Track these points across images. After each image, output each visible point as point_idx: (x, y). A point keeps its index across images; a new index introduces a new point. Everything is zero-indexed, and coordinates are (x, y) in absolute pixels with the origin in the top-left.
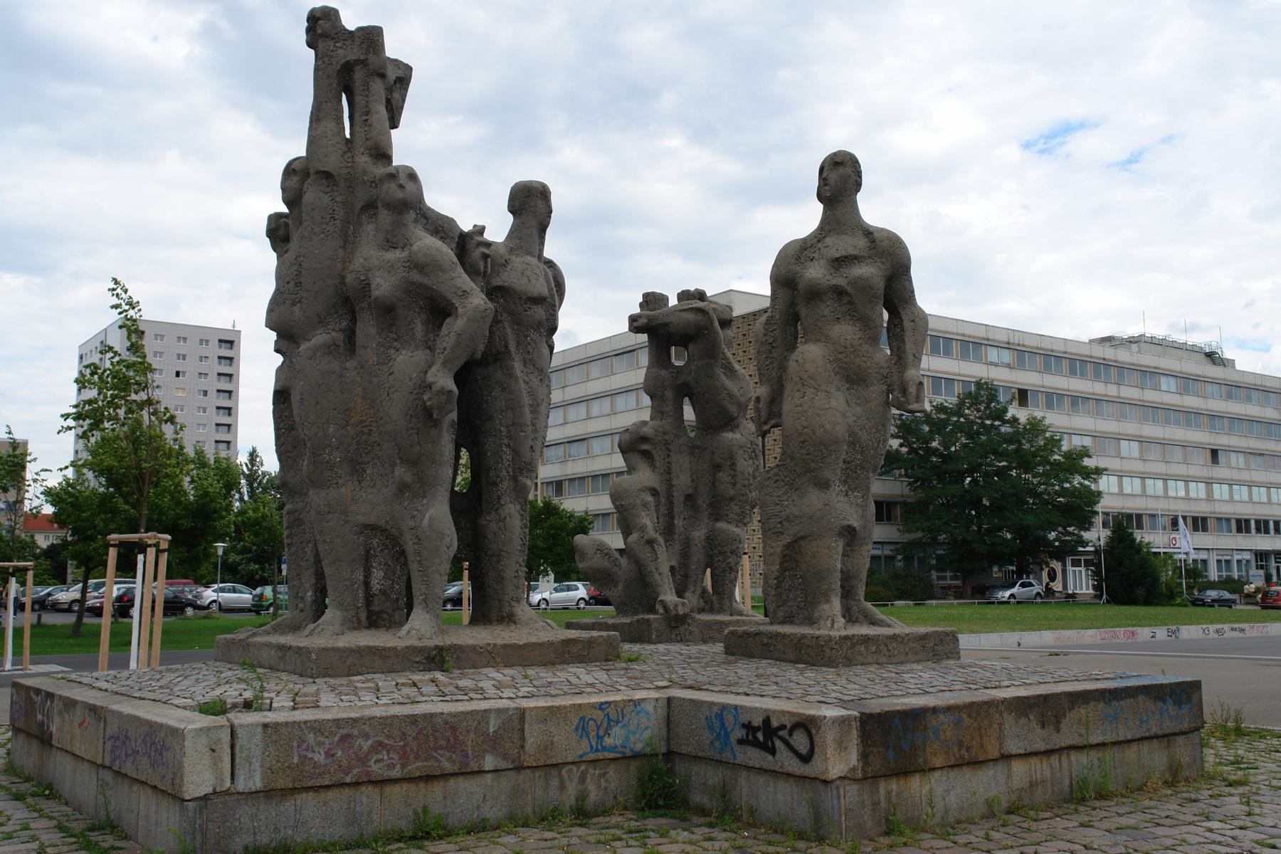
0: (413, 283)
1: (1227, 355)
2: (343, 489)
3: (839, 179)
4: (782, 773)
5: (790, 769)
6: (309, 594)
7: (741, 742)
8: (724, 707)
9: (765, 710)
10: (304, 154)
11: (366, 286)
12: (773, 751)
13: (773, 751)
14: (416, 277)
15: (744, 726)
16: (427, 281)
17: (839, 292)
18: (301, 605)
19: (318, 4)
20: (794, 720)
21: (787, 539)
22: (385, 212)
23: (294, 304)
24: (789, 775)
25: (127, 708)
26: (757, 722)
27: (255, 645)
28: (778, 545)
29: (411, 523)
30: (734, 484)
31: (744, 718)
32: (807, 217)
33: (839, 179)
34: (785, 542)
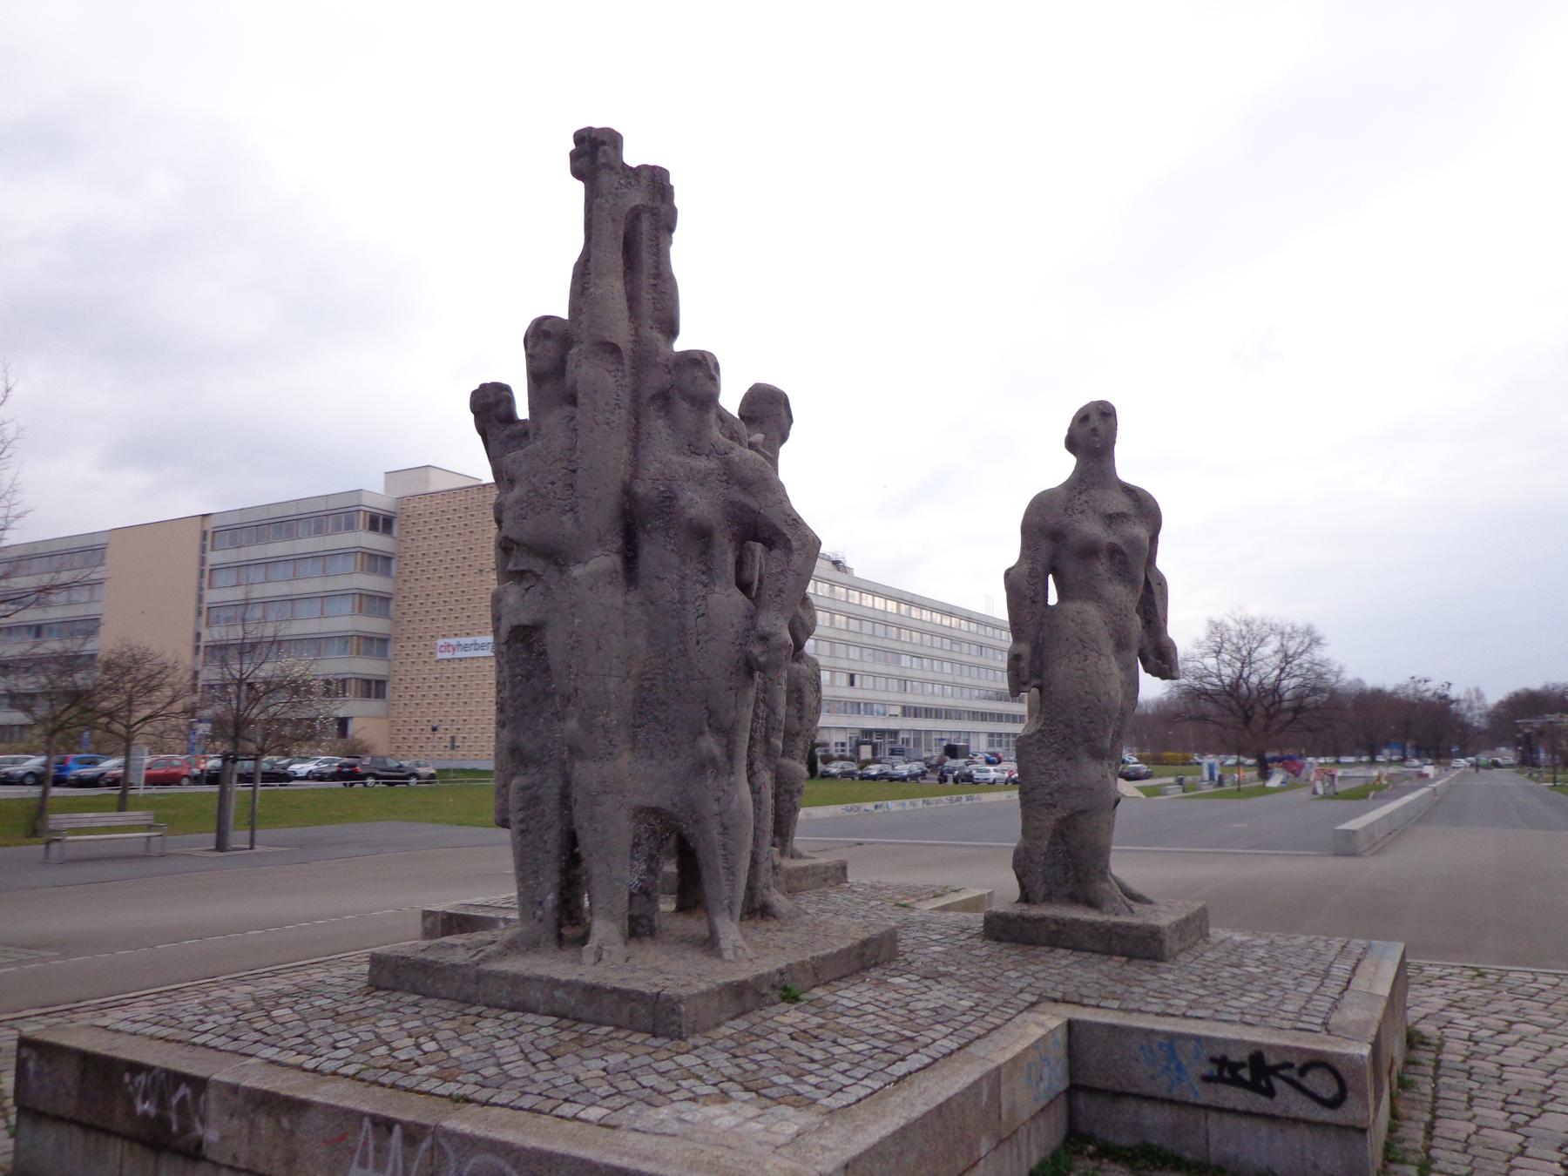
0: (733, 504)
1: (848, 564)
2: (619, 761)
3: (1092, 433)
4: (1288, 1119)
5: (1302, 1114)
6: (551, 897)
7: (1207, 1079)
8: (1172, 1037)
9: (1253, 1044)
10: (563, 312)
11: (669, 498)
12: (1270, 1093)
13: (1270, 1093)
14: (738, 495)
15: (1213, 1060)
16: (754, 504)
17: (1114, 551)
18: (539, 913)
19: (598, 124)
20: (1306, 1059)
21: (1061, 814)
22: (686, 406)
23: (564, 513)
24: (1296, 1121)
25: (462, 1123)
26: (1236, 1056)
27: (489, 974)
28: (1049, 821)
29: (715, 807)
30: (800, 718)
31: (1218, 1052)
32: (1060, 467)
33: (1092, 433)
34: (1059, 816)
